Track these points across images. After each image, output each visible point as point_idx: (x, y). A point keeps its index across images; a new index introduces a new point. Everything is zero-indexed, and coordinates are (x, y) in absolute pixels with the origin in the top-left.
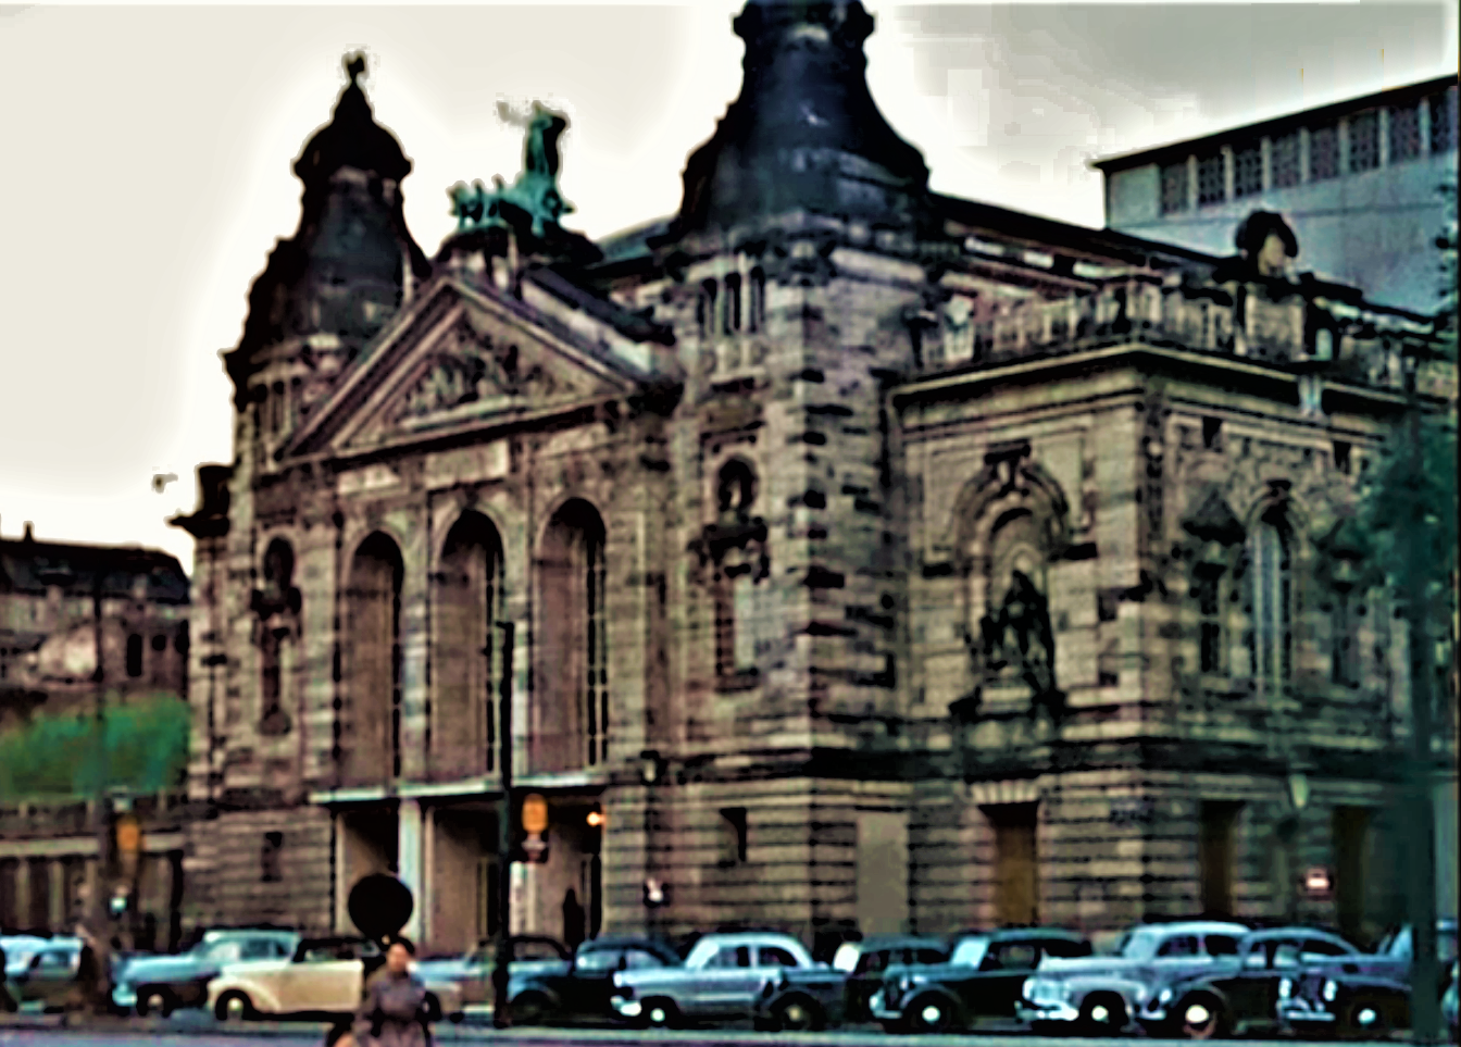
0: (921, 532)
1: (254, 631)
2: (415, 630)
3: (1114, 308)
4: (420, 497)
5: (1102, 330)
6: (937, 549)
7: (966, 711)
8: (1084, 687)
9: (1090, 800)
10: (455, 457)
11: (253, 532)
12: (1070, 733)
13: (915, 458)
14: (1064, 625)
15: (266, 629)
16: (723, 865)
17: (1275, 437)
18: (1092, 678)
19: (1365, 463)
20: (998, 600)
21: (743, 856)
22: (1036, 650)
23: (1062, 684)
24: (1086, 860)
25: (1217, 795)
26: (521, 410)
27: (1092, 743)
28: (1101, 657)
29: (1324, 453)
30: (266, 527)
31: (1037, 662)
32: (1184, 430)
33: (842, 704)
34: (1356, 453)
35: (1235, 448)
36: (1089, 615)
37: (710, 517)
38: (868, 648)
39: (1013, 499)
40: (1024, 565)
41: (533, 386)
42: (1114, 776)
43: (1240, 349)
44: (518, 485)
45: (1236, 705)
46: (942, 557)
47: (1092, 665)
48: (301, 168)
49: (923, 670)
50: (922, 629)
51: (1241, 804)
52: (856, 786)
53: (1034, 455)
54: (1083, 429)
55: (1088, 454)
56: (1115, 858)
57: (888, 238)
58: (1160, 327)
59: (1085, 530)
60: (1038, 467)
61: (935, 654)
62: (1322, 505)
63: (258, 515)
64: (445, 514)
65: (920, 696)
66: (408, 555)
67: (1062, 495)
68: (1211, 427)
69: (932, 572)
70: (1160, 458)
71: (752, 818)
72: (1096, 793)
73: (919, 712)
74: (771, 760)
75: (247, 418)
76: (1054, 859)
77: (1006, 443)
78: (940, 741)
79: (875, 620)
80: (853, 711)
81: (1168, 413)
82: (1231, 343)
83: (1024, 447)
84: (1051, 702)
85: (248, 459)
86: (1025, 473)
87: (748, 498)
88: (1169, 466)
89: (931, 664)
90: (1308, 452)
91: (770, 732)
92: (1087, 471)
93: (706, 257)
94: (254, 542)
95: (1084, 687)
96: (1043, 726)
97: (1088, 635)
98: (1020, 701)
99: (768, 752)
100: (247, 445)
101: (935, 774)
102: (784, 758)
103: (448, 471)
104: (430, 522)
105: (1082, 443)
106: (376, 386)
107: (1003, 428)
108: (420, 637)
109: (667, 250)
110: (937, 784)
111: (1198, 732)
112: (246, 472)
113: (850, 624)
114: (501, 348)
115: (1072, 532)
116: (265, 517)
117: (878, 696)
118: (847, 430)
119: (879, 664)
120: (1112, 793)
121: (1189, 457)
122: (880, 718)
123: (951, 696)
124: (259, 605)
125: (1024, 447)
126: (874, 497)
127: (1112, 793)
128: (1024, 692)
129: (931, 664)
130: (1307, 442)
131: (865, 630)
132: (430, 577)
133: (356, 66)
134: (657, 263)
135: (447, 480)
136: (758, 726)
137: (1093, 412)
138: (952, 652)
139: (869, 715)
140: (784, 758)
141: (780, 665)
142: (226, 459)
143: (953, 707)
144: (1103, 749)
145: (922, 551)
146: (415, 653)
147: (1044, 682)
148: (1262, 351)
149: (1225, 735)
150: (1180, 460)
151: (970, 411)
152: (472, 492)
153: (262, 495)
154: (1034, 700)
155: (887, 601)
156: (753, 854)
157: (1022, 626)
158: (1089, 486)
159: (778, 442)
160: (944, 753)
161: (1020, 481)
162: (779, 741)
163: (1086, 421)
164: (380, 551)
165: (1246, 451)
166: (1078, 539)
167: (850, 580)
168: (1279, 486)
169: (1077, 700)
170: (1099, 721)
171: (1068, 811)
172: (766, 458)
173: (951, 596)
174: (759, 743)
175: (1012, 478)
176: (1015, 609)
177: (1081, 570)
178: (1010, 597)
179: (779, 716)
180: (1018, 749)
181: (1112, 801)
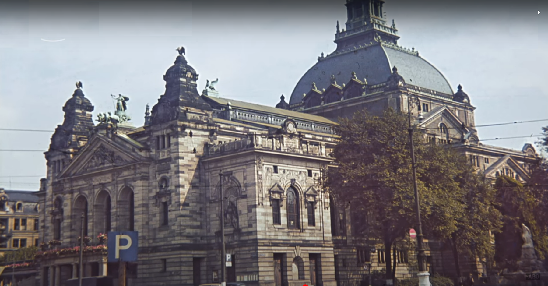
0: (209, 192)
1: (52, 219)
2: (90, 218)
3: (250, 141)
4: (92, 187)
5: (247, 146)
6: (212, 196)
7: (219, 234)
8: (245, 228)
9: (246, 254)
10: (98, 178)
11: (52, 196)
12: (243, 238)
13: (208, 176)
14: (241, 214)
15: (55, 219)
16: (161, 272)
17: (292, 169)
18: (247, 226)
19: (316, 174)
20: (227, 208)
21: (164, 271)
22: (235, 219)
23: (240, 227)
24: (246, 268)
25: (277, 252)
26: (114, 166)
27: (246, 241)
28: (248, 221)
29: (305, 172)
30: (55, 194)
31: (235, 222)
32: (268, 169)
33: (189, 233)
34: (313, 172)
35: (282, 172)
36: (246, 211)
37: (158, 190)
38: (196, 220)
39: (229, 184)
40: (232, 200)
41: (118, 161)
42: (251, 248)
43: (282, 150)
44: (115, 183)
45: (282, 230)
46: (213, 198)
47: (246, 223)
48: (165, 78)
49: (210, 224)
50: (209, 215)
51: (203, 258)
52: (193, 252)
53: (233, 175)
54: (244, 169)
55: (245, 174)
56: (252, 267)
57: (200, 126)
58: (262, 145)
59: (244, 192)
60: (234, 178)
61: (212, 221)
62: (305, 184)
63: (53, 192)
64: (97, 191)
65: (209, 231)
66: (89, 200)
67: (239, 183)
68: (275, 168)
69: (211, 202)
70: (261, 175)
71: (168, 261)
72: (248, 252)
73: (209, 234)
74: (172, 246)
75: (51, 169)
76: (240, 268)
77: (227, 172)
78: (213, 241)
79: (197, 214)
80: (192, 234)
81: (263, 165)
82: (280, 148)
83: (231, 173)
84: (238, 231)
85: (51, 178)
86: (231, 179)
87: (167, 186)
88: (264, 177)
89: (212, 223)
90: (300, 172)
91: (172, 240)
92: (245, 178)
93: (157, 131)
94: (52, 198)
95: (245, 228)
96: (236, 237)
97: (246, 215)
98: (230, 231)
99: (171, 245)
100: (51, 175)
101: (212, 249)
102: (175, 246)
103: (98, 181)
104: (94, 192)
105: (244, 172)
106: (83, 159)
107: (226, 169)
108: (91, 220)
109: (148, 130)
110: (213, 251)
111: (273, 237)
112: (50, 182)
113: (191, 215)
114: (110, 152)
115: (242, 192)
116: (55, 192)
117: (198, 231)
118: (189, 170)
119: (199, 223)
120: (251, 252)
121: (269, 174)
122: (199, 236)
123: (215, 230)
124: (53, 213)
125: (231, 173)
126: (197, 185)
127: (251, 252)
128: (232, 229)
129: (212, 223)
130: (300, 170)
131: (194, 216)
132: (94, 206)
133: (182, 51)
134: (146, 132)
135: (97, 183)
136: (169, 239)
137: (246, 165)
138: (216, 220)
139: (196, 235)
140: (175, 246)
141: (174, 225)
142: (45, 177)
143: (216, 233)
144: (248, 242)
145: (209, 197)
146: (90, 225)
147: (236, 227)
148: (288, 150)
149: (279, 238)
150: (267, 175)
151: (219, 165)
152: (103, 185)
153: (55, 186)
154: (234, 231)
155: (201, 209)
156: (168, 269)
157: (231, 213)
158: (245, 182)
159: (173, 173)
160: (214, 244)
161: (230, 181)
162: (173, 242)
163: (244, 167)
164: (82, 199)
165: (284, 172)
166: (243, 194)
167: (190, 204)
168: (293, 181)
169: (244, 230)
170: (248, 235)
171: (242, 257)
172: (171, 177)
173: (215, 207)
174: (169, 243)
175: (229, 180)
176: (230, 210)
177: (244, 201)
178: (229, 207)
179: (174, 236)
180: (230, 243)
181: (251, 254)
